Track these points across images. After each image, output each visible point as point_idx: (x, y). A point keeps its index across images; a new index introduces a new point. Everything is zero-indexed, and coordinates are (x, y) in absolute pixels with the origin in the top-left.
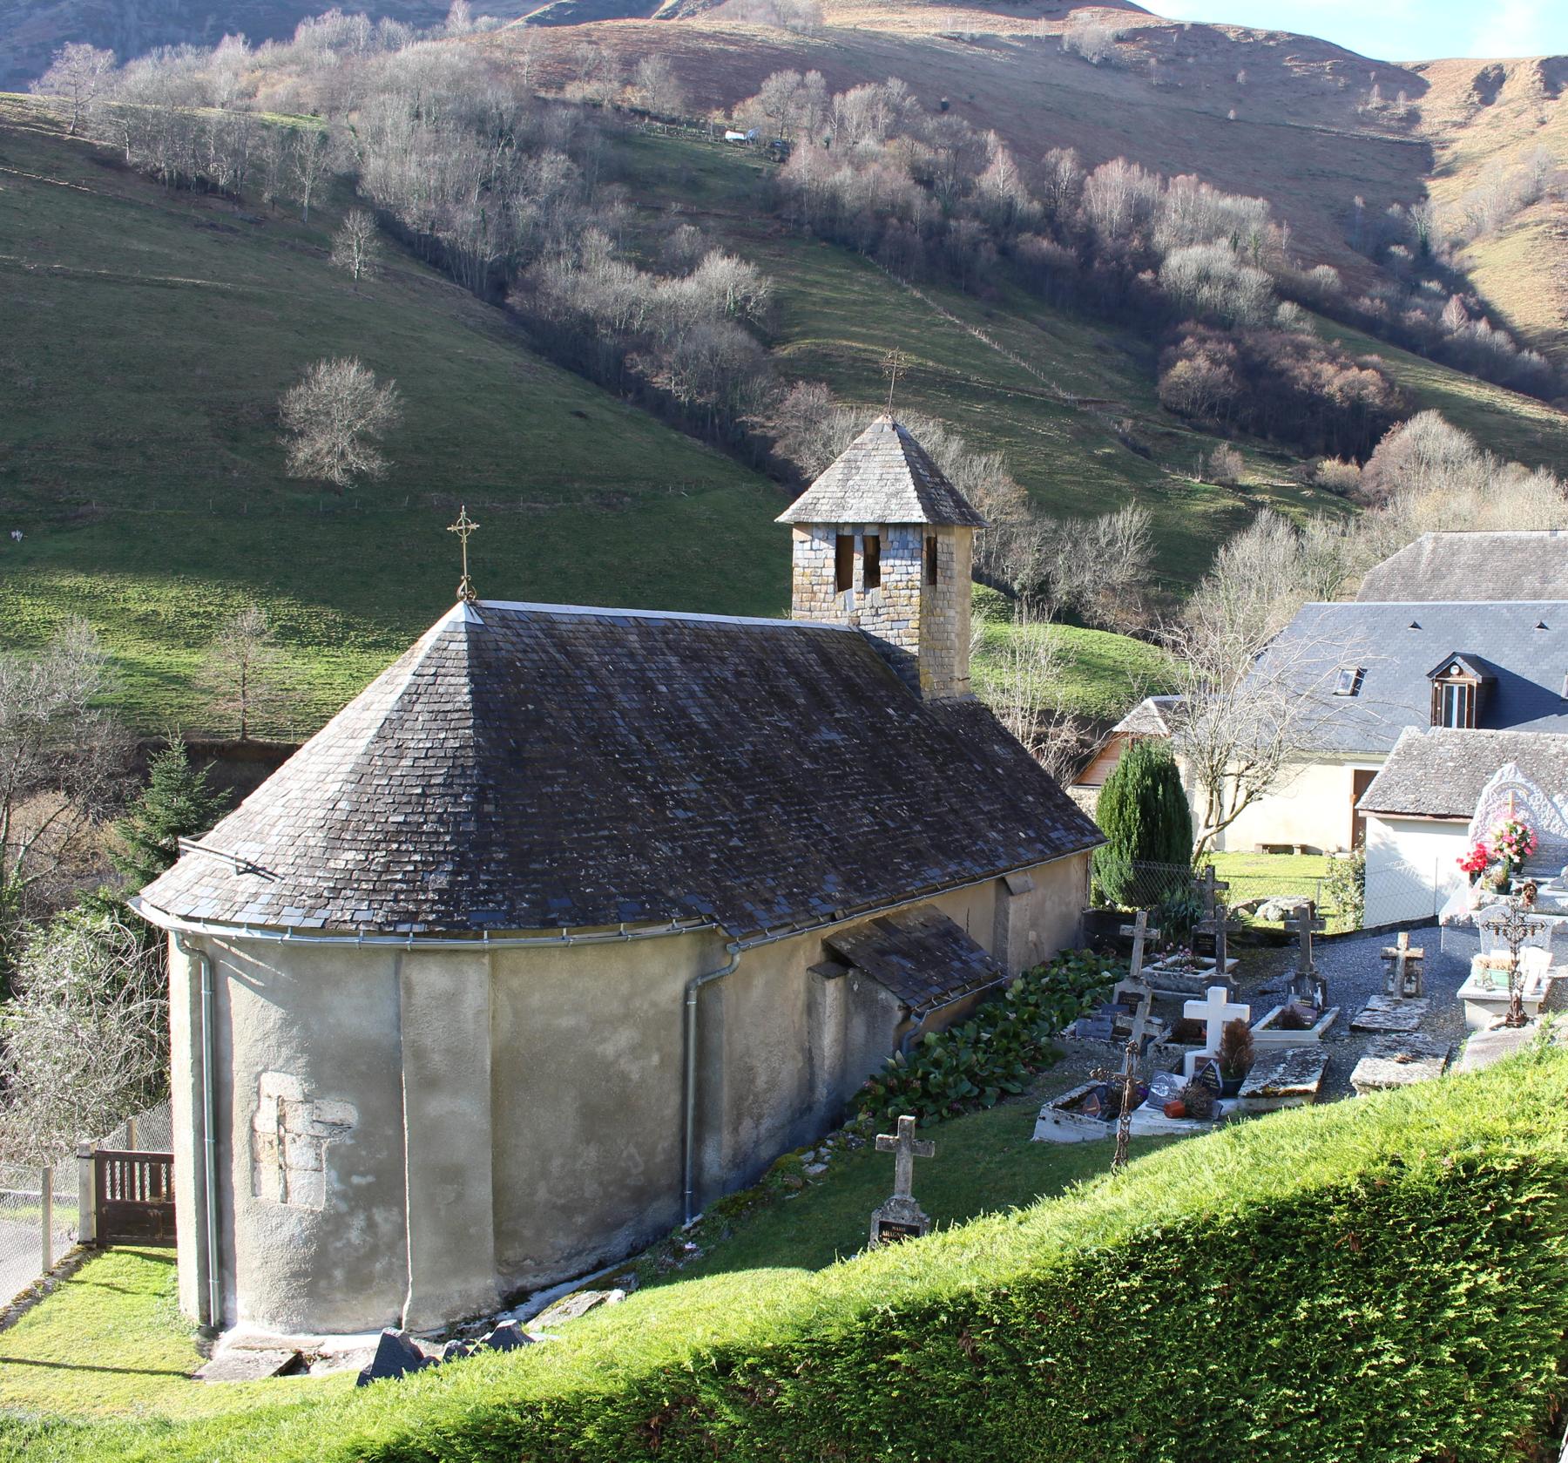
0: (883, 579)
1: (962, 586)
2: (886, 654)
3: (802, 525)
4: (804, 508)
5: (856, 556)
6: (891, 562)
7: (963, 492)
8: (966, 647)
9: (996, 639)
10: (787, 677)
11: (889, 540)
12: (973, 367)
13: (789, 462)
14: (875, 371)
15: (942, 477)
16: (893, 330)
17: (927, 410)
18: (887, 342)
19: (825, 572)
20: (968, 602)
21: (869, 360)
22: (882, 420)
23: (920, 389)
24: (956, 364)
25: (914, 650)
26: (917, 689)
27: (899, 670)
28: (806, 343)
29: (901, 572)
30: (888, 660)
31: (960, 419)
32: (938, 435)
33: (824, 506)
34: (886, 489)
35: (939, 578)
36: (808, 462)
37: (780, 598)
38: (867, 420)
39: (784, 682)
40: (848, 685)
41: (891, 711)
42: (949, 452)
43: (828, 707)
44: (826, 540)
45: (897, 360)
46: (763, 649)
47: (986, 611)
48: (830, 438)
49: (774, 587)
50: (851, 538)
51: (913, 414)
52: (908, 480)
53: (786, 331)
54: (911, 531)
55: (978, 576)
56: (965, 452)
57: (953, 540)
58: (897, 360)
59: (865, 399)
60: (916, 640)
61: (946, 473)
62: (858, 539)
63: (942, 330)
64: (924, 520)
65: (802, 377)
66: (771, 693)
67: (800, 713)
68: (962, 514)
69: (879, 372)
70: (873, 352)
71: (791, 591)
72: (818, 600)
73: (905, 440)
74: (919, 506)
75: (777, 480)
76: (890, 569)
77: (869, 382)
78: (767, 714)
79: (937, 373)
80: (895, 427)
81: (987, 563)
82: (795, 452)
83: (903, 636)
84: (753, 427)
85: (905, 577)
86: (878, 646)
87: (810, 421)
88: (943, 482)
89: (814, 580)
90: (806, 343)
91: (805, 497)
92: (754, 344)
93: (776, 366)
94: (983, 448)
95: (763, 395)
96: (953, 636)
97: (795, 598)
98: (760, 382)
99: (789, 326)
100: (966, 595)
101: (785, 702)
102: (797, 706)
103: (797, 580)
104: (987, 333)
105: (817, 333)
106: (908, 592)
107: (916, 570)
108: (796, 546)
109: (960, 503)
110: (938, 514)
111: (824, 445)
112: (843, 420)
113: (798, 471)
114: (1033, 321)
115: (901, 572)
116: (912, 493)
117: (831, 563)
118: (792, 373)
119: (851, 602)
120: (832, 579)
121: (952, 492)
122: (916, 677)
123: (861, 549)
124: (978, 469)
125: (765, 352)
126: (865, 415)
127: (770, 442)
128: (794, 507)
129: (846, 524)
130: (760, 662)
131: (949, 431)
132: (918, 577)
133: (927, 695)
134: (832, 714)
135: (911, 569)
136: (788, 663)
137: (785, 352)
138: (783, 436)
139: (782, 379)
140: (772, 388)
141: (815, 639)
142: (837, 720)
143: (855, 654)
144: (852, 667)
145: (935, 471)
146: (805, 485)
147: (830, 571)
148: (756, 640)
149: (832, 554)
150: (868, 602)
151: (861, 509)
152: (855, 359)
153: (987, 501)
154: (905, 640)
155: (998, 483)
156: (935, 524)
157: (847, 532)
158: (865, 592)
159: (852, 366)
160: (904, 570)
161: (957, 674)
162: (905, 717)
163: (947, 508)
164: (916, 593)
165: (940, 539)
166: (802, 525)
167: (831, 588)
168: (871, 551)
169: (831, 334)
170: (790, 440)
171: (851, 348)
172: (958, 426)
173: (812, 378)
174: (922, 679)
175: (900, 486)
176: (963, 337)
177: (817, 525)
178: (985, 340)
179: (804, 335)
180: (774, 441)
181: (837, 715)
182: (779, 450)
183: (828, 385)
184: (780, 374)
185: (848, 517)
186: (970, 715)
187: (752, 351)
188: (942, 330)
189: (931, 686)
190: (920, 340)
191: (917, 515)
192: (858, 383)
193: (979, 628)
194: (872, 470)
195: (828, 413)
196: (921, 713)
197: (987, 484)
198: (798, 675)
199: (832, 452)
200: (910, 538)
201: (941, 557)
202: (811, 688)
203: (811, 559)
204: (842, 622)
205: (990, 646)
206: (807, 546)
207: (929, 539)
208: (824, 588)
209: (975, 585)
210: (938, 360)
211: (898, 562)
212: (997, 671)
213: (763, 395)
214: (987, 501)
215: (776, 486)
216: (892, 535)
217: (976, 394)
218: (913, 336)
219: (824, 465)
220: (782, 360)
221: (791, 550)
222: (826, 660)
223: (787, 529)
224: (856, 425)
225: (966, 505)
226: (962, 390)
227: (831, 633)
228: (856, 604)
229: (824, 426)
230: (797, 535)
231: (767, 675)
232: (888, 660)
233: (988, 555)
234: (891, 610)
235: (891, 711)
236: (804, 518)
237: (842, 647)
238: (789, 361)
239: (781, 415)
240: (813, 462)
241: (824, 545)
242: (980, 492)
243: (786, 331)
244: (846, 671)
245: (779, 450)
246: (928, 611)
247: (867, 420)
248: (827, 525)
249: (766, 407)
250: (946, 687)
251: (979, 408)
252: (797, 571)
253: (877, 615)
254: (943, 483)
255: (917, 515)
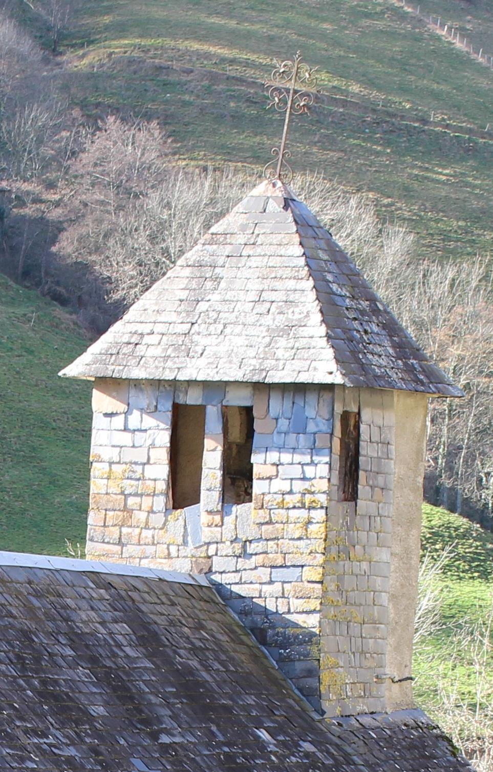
0: (258, 487)
1: (399, 501)
2: (262, 631)
3: (108, 383)
4: (114, 353)
5: (209, 443)
6: (273, 456)
7: (411, 331)
8: (409, 621)
9: (463, 610)
10: (73, 665)
11: (272, 415)
12: (436, 96)
13: (85, 268)
14: (250, 101)
15: (373, 299)
16: (287, 24)
17: (347, 175)
18: (274, 46)
19: (150, 472)
20: (414, 543)
21: (240, 80)
22: (266, 191)
23: (345, 135)
24: (403, 90)
25: (311, 622)
26: (313, 695)
27: (281, 660)
28: (122, 46)
29: (293, 474)
30: (263, 641)
31: (407, 193)
32: (365, 225)
33: (152, 350)
34: (268, 320)
35: (363, 489)
36: (118, 268)
37: (65, 522)
38: (234, 193)
39: (68, 674)
40: (189, 688)
41: (264, 735)
42: (386, 257)
43: (146, 722)
44: (154, 411)
45: (296, 78)
46: (30, 611)
47: (445, 558)
48: (163, 226)
49: (57, 504)
50: (200, 410)
51: (322, 184)
52: (309, 303)
53: (88, 21)
54: (312, 398)
55: (434, 493)
56: (415, 257)
57: (390, 418)
58: (296, 78)
59: (230, 153)
60: (315, 604)
61: (381, 293)
62: (213, 415)
63: (380, 24)
64: (338, 379)
65: (115, 110)
66: (43, 695)
67: (96, 734)
68: (410, 369)
69: (258, 102)
70: (247, 64)
71: (84, 510)
72: (135, 526)
73: (308, 229)
74: (330, 353)
75: (63, 301)
76: (270, 471)
77: (237, 119)
78: (35, 732)
79: (367, 106)
80: (288, 203)
81: (450, 468)
82: (97, 250)
83: (292, 596)
84: (20, 201)
85: (299, 486)
86: (244, 613)
87: (127, 193)
88: (375, 310)
89: (130, 486)
90: (122, 46)
91: (117, 332)
92: (26, 45)
93: (65, 88)
94: (446, 248)
95: (40, 141)
96: (384, 598)
97: (93, 518)
98: (37, 116)
99: (93, 13)
100: (412, 522)
101: (67, 710)
102: (91, 719)
103: (97, 485)
104: (463, 32)
105: (144, 27)
106: (303, 514)
107: (321, 472)
108: (98, 422)
109: (406, 350)
110: (364, 368)
111: (152, 239)
112: (188, 192)
113: (101, 287)
114: (98, 714)
115: (293, 474)
116: (316, 329)
117: (162, 456)
118: (94, 103)
119: (196, 532)
120: (162, 486)
121: (392, 328)
122: (313, 673)
123: (217, 436)
124: (439, 289)
125: (46, 61)
126: (230, 183)
127: (50, 231)
128: (96, 348)
129: (190, 383)
130: (26, 635)
131: (385, 217)
132: (324, 485)
133: (332, 707)
134: (154, 736)
135: (310, 471)
136: (76, 639)
137: (81, 61)
138: (76, 219)
139: (76, 113)
140: (57, 128)
141: (126, 597)
142: (165, 748)
143: (200, 626)
144: (194, 650)
145: (361, 289)
146: (116, 312)
147: (160, 470)
148: (18, 595)
149: (164, 438)
150: (228, 531)
151: (224, 355)
152: (214, 78)
153: (454, 351)
154: (296, 604)
155: (476, 316)
156: (358, 387)
157: (193, 398)
158: (223, 513)
159: (208, 91)
160: (296, 471)
161: (390, 670)
162: (291, 747)
163: (381, 358)
164: (319, 515)
165: (366, 415)
166: (108, 383)
167: (160, 503)
168: (236, 434)
169: (171, 28)
170: (88, 227)
171: (207, 56)
172: (404, 209)
173: (133, 112)
174: (325, 676)
175: (294, 315)
176: (417, 39)
177: (137, 384)
178: (459, 44)
179: (120, 30)
180: (59, 228)
181: (165, 739)
182: (66, 246)
183: (163, 124)
184: (73, 104)
185: (197, 369)
186: (411, 747)
187: (22, 58)
188: (380, 24)
189: (343, 693)
190: (336, 43)
191: (324, 368)
192: (221, 122)
193: (433, 588)
194: (242, 282)
195: (161, 178)
196: (321, 740)
197: (454, 318)
198: (94, 661)
199: (166, 252)
200: (310, 412)
201: (367, 451)
202: (118, 687)
203: (125, 446)
204: (179, 567)
205: (448, 623)
206: (118, 421)
207: (345, 416)
208: (147, 502)
209: (426, 507)
210: (370, 82)
211: (286, 457)
212: (461, 671)
213: (40, 141)
214: (454, 351)
215: (59, 312)
216: (277, 405)
217: (438, 148)
218: (323, 36)
219: (150, 275)
220: (76, 77)
221: (86, 434)
222: (148, 637)
223: (81, 391)
224: (212, 202)
225: (417, 353)
226: (407, 137)
227: (160, 587)
228: (207, 534)
229: (152, 202)
230: (101, 401)
231: (38, 660)
232: (263, 641)
233: (453, 452)
234: (270, 549)
235: (264, 735)
236: (113, 370)
237: (176, 612)
238: (91, 78)
239: (73, 179)
240: (130, 269)
241: (149, 421)
242: (441, 334)
243: (88, 21)
244: (185, 659)
245: (66, 246)
246: (339, 549)
247: (234, 193)
248: (156, 384)
249: (46, 167)
250: (367, 694)
251: (443, 173)
252: (97, 470)
253: (244, 554)
254: (376, 311)
255: (324, 368)
